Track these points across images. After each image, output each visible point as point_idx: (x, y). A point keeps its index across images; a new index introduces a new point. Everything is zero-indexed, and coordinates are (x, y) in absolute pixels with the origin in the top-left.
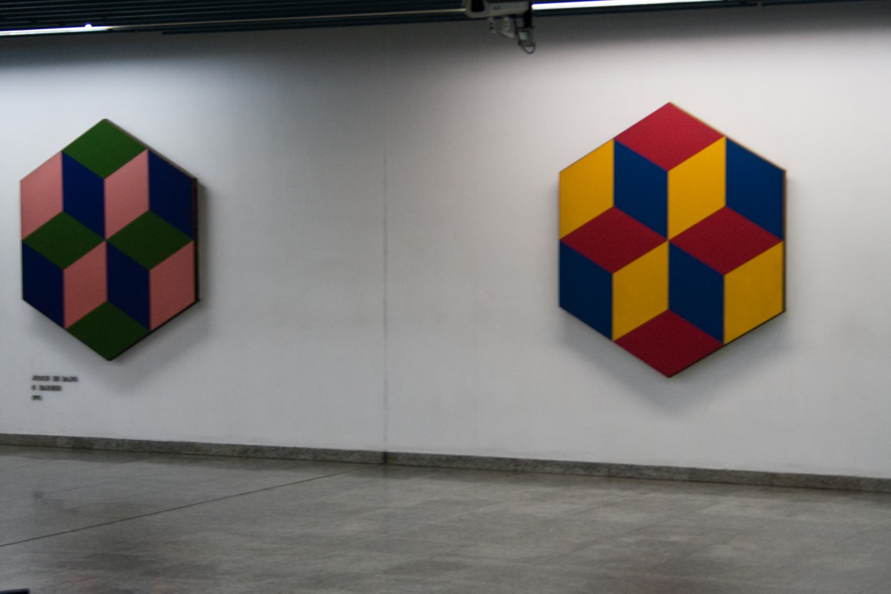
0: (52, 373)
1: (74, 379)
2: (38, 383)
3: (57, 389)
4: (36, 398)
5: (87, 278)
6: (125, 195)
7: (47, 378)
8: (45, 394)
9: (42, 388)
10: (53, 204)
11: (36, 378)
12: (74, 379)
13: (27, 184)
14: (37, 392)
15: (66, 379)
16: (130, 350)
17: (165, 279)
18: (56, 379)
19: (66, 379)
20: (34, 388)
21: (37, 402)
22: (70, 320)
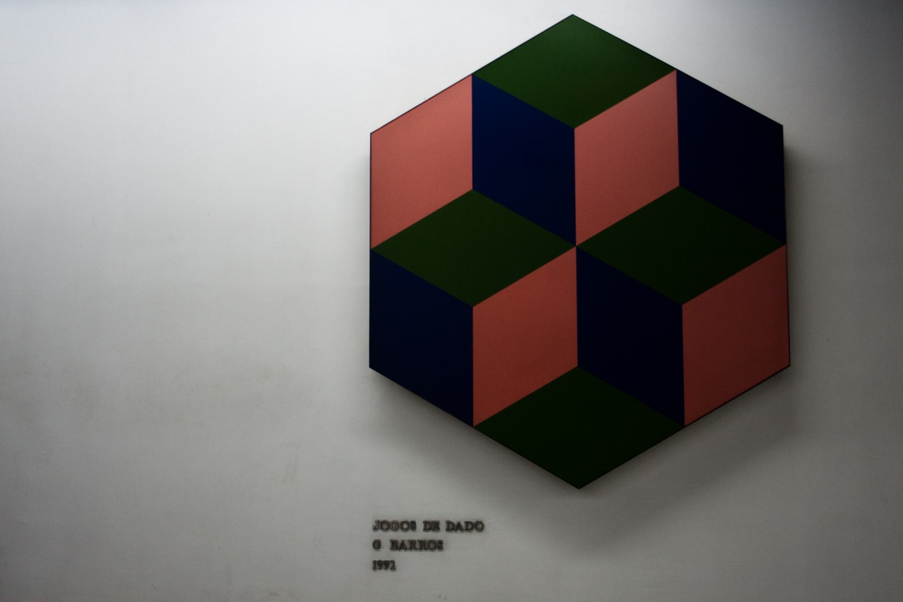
0: (420, 515)
1: (476, 526)
2: (387, 537)
3: (438, 545)
4: (380, 565)
5: (528, 323)
6: (619, 162)
7: (412, 525)
8: (400, 557)
9: (396, 546)
10: (449, 174)
11: (381, 525)
12: (476, 526)
13: (382, 141)
14: (385, 554)
15: (453, 527)
16: (791, 341)
17: (707, 321)
18: (432, 526)
19: (453, 527)
20: (377, 545)
21: (383, 573)
22: (482, 411)
